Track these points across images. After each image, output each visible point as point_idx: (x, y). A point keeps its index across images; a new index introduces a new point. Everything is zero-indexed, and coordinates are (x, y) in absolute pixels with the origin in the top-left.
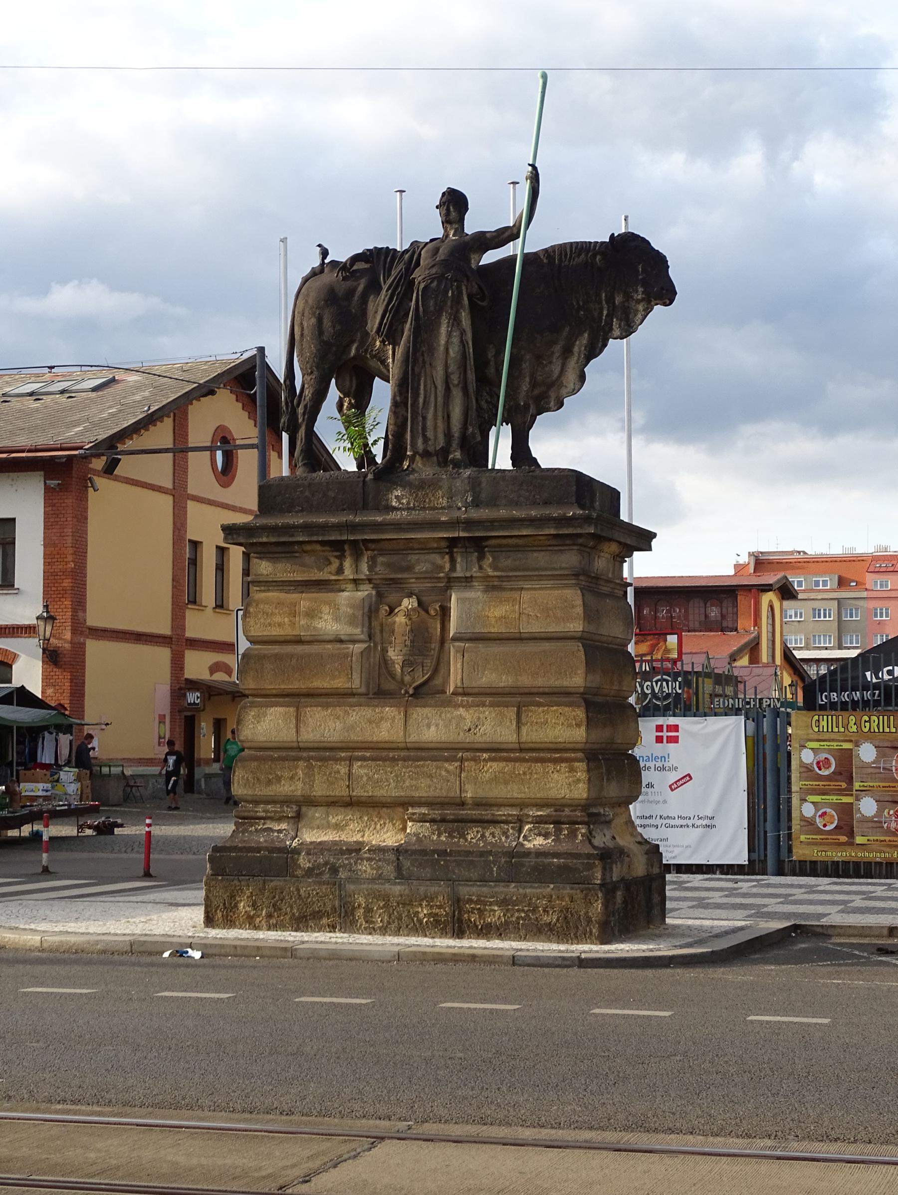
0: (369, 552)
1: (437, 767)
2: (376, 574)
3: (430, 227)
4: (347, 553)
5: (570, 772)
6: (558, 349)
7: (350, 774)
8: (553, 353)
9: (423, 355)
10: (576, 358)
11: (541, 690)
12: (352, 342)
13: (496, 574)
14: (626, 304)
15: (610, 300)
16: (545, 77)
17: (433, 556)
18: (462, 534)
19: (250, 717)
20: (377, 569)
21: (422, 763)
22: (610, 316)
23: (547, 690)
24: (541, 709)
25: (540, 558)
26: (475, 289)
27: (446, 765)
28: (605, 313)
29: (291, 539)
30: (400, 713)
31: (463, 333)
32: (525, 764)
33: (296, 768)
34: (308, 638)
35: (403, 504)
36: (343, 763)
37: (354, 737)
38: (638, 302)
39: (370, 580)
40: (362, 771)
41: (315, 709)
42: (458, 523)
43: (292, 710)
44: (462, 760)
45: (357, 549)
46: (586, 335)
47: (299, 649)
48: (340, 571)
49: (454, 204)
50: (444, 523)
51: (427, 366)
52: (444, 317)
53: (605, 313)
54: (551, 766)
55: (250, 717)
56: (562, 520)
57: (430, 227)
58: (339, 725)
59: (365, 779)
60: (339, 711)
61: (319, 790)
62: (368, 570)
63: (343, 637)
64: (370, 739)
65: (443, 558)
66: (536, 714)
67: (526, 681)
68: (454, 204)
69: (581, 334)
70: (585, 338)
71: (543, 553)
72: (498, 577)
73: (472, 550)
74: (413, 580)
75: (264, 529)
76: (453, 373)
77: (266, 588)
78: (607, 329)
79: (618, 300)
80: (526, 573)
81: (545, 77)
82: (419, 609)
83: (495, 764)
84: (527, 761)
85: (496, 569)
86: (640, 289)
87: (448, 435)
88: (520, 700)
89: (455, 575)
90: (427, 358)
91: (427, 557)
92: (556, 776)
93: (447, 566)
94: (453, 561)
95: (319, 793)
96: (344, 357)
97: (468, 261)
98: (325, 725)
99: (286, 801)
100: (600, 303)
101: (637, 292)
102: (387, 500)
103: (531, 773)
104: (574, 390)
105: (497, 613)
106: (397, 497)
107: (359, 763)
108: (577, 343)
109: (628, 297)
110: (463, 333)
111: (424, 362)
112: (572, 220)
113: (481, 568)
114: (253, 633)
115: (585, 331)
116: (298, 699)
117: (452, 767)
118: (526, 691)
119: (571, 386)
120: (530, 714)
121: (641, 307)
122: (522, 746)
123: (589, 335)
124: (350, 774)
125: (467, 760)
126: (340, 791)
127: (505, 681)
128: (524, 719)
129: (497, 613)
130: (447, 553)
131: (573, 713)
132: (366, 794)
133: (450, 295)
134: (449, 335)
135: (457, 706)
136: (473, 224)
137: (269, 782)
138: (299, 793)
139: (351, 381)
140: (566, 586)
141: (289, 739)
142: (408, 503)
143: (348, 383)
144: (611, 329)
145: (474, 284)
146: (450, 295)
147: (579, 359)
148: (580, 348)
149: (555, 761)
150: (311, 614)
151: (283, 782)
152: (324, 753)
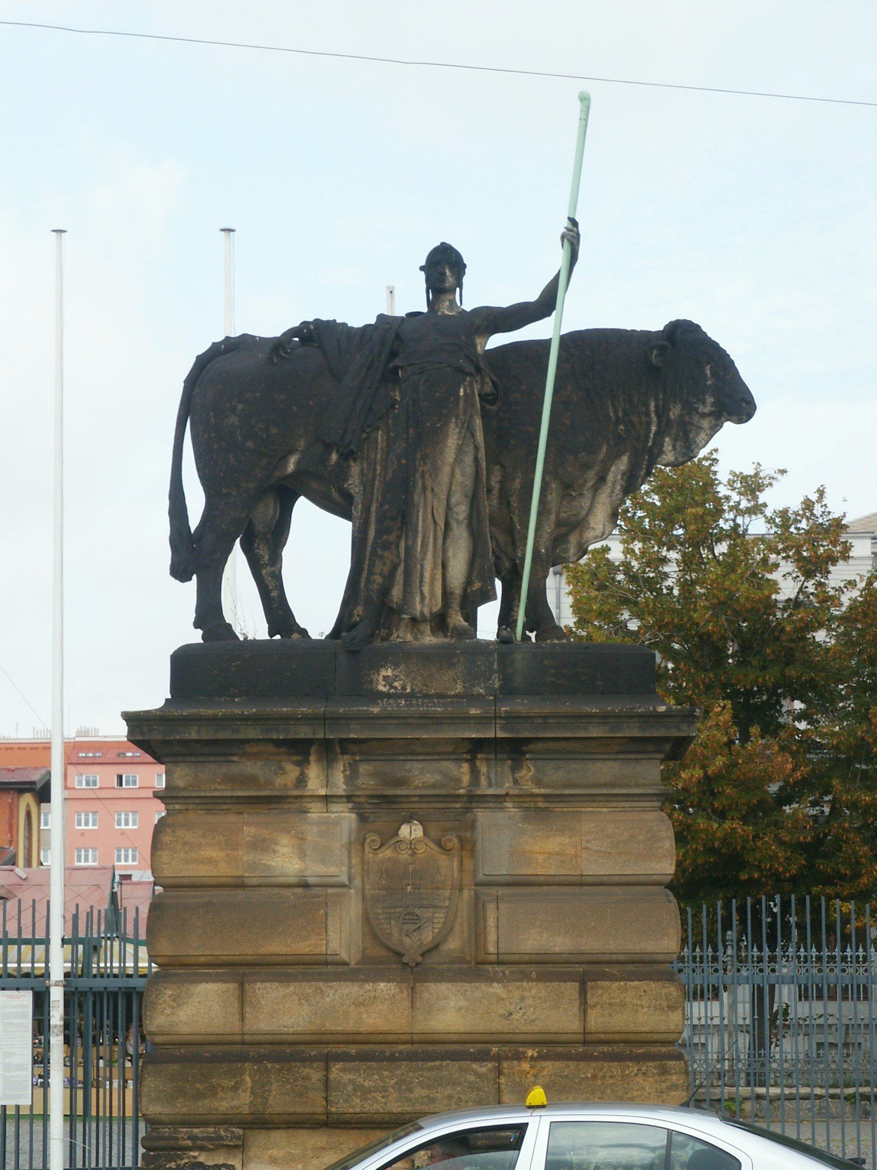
0: (346, 757)
1: (461, 1070)
2: (360, 789)
3: (412, 298)
4: (312, 758)
5: (661, 1074)
6: (591, 476)
7: (326, 1082)
8: (586, 481)
9: (423, 476)
10: (609, 490)
11: (614, 957)
12: (291, 452)
13: (543, 791)
14: (687, 419)
15: (662, 413)
16: (585, 99)
17: (446, 764)
18: (500, 734)
19: (166, 998)
20: (359, 782)
21: (438, 1063)
22: (660, 434)
23: (622, 958)
24: (617, 984)
25: (605, 770)
26: (488, 388)
27: (475, 1066)
28: (654, 428)
29: (235, 737)
30: (402, 991)
31: (476, 448)
32: (594, 1064)
33: (242, 1073)
34: (255, 881)
35: (396, 688)
36: (315, 1065)
37: (329, 1026)
38: (703, 416)
39: (349, 798)
40: (346, 1077)
41: (268, 985)
42: (495, 718)
43: (232, 986)
44: (498, 1058)
45: (329, 750)
46: (625, 459)
47: (240, 895)
48: (302, 781)
49: (444, 267)
50: (475, 717)
51: (429, 494)
52: (453, 425)
53: (654, 428)
54: (633, 1068)
55: (166, 998)
56: (649, 716)
57: (412, 298)
58: (306, 1009)
59: (350, 1088)
60: (308, 988)
61: (279, 1101)
62: (346, 783)
63: (311, 880)
64: (356, 1029)
65: (461, 767)
66: (606, 993)
67: (592, 943)
68: (444, 267)
69: (618, 456)
70: (623, 464)
71: (610, 763)
72: (545, 796)
73: (505, 756)
74: (416, 799)
75: (187, 721)
76: (457, 504)
77: (184, 807)
78: (655, 451)
79: (675, 412)
80: (590, 791)
81: (585, 99)
82: (427, 841)
83: (548, 1064)
84: (596, 1059)
85: (539, 783)
86: (710, 400)
87: (447, 594)
88: (585, 973)
89: (479, 792)
90: (429, 483)
91: (435, 765)
92: (640, 1079)
93: (466, 779)
94: (475, 772)
95: (278, 1110)
96: (277, 474)
97: (474, 346)
98: (284, 1010)
99: (227, 1121)
100: (648, 414)
101: (704, 403)
102: (371, 682)
103: (604, 1077)
104: (603, 533)
105: (547, 850)
106: (385, 678)
107: (340, 1065)
108: (613, 468)
109: (689, 409)
110: (476, 448)
111: (424, 487)
112: (613, 300)
113: (516, 782)
114: (166, 873)
115: (624, 454)
116: (242, 972)
117: (484, 1068)
118: (591, 958)
119: (600, 528)
120: (600, 992)
121: (705, 423)
122: (589, 1037)
123: (629, 458)
124: (326, 1082)
125: (507, 1058)
126: (315, 1105)
127: (560, 943)
128: (591, 1000)
129: (547, 850)
130: (467, 760)
131: (664, 991)
132: (351, 1110)
133: (462, 394)
134: (460, 451)
135: (490, 980)
136: (474, 295)
137: (200, 1095)
138: (246, 1110)
139: (275, 510)
140: (644, 810)
141: (228, 1030)
142: (404, 688)
143: (271, 511)
144: (661, 452)
145: (488, 379)
146: (462, 394)
147: (612, 491)
148: (615, 477)
149: (637, 1059)
150: (262, 845)
151: (221, 1094)
152: (283, 1053)
